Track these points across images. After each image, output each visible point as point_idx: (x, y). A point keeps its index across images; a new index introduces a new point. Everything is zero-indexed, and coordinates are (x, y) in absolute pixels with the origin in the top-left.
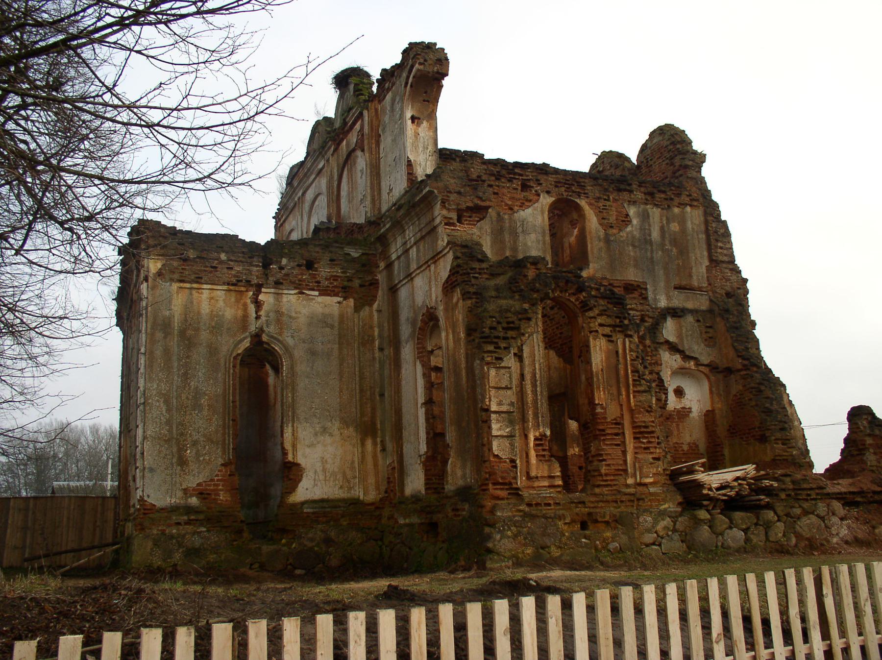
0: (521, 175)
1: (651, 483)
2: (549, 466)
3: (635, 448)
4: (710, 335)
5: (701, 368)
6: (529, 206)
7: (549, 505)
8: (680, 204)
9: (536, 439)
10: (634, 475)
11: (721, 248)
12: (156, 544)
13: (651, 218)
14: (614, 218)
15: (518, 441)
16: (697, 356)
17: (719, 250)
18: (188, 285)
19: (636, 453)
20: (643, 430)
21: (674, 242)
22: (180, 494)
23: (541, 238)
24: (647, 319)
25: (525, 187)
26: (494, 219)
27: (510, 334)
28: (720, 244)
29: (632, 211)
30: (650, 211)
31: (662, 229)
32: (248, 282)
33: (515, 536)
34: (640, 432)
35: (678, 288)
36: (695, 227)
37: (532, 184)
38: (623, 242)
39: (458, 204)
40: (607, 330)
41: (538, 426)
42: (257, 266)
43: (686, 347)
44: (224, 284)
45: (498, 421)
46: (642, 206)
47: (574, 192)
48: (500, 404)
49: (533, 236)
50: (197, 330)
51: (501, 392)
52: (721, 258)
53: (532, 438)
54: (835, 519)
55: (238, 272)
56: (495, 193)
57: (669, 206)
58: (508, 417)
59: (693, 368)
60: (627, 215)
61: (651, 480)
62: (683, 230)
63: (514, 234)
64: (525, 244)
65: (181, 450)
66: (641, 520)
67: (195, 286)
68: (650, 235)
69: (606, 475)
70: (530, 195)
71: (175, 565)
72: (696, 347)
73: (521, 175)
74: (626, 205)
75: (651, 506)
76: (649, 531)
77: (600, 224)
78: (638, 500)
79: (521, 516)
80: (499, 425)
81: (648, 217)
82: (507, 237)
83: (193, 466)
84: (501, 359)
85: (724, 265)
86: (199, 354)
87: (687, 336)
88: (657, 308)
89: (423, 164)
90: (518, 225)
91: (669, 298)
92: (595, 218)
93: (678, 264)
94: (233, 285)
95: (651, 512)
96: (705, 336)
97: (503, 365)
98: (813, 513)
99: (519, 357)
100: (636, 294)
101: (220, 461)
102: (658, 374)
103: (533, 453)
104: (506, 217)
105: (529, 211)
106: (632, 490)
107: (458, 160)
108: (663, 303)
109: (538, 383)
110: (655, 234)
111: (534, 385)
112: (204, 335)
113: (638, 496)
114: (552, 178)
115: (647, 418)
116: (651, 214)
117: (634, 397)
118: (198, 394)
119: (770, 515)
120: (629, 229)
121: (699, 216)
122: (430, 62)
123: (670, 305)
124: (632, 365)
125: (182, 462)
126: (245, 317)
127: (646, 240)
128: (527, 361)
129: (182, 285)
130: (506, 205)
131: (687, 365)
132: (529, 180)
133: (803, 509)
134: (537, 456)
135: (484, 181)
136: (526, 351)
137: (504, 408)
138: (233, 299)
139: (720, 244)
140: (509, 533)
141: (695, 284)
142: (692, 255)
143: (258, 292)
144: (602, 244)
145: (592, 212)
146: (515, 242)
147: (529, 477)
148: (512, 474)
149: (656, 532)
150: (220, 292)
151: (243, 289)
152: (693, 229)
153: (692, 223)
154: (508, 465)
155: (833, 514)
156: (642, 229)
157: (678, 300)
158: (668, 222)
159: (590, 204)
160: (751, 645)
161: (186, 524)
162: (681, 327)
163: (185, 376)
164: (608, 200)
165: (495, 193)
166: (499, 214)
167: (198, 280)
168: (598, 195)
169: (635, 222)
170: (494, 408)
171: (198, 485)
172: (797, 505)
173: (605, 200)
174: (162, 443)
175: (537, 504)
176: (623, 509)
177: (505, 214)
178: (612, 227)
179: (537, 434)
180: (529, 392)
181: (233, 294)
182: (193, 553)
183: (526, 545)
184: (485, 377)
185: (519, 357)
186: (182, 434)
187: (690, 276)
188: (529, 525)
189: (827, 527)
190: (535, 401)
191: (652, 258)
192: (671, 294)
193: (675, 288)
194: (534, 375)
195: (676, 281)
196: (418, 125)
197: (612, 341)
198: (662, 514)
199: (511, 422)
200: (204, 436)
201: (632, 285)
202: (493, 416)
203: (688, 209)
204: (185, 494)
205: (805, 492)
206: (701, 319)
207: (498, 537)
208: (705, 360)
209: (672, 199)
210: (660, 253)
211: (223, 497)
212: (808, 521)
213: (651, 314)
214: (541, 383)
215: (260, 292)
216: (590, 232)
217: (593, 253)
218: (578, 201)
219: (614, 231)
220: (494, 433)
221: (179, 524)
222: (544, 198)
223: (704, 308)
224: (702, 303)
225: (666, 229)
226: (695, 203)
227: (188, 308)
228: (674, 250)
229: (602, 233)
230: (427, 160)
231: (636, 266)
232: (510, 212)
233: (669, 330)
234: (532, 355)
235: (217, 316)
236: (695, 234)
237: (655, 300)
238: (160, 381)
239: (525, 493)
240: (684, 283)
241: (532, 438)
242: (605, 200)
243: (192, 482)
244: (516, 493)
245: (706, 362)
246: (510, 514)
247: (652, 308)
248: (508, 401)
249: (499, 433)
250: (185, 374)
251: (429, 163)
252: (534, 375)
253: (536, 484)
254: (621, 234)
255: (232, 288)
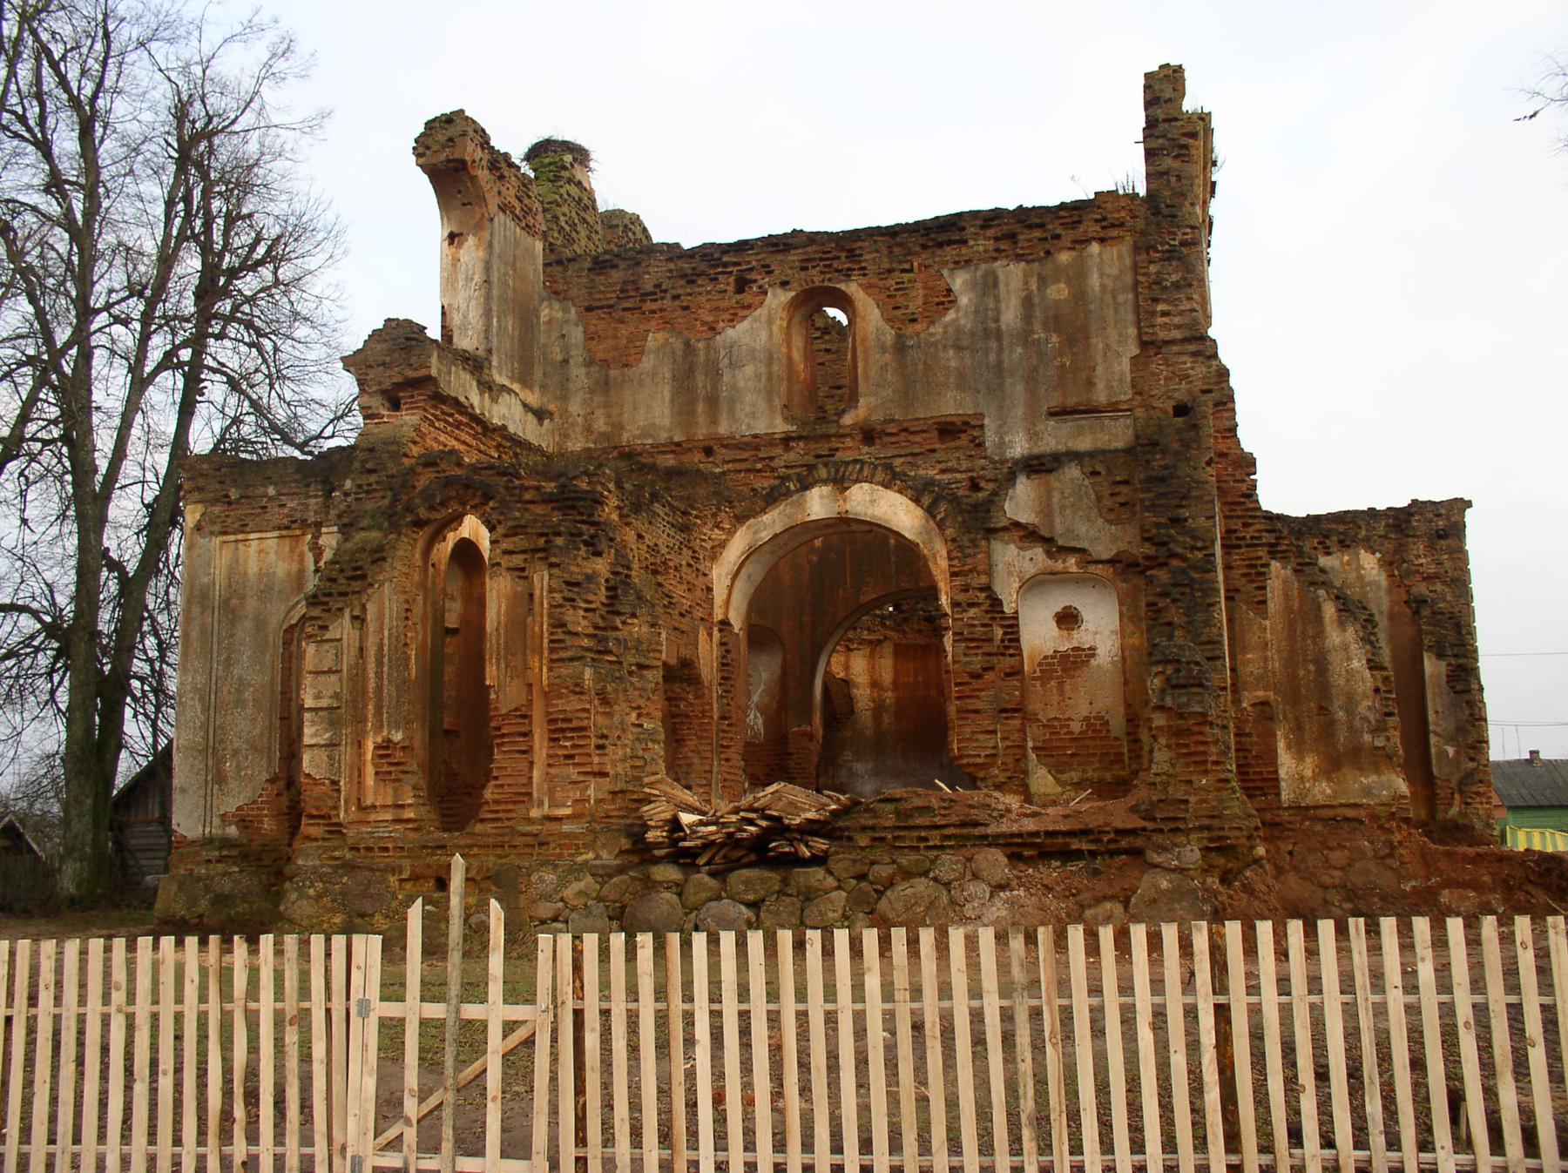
0: (738, 264)
1: (568, 817)
2: (395, 790)
3: (550, 756)
4: (1121, 499)
5: (1097, 569)
6: (745, 317)
7: (386, 849)
8: (1076, 242)
9: (377, 747)
10: (541, 804)
11: (1164, 314)
12: (181, 886)
13: (1002, 287)
14: (920, 302)
15: (346, 753)
16: (1085, 545)
17: (1160, 320)
18: (232, 538)
19: (549, 765)
20: (560, 725)
21: (1055, 322)
22: (216, 821)
23: (763, 369)
24: (983, 484)
25: (742, 285)
26: (680, 353)
27: (356, 585)
28: (1160, 307)
29: (959, 281)
30: (1000, 272)
31: (1027, 302)
32: (304, 521)
33: (319, 897)
34: (559, 729)
35: (1058, 413)
36: (1110, 285)
37: (753, 276)
38: (935, 344)
39: (380, 383)
40: (518, 560)
41: (382, 727)
42: (316, 496)
43: (1059, 528)
44: (274, 529)
45: (313, 723)
46: (983, 267)
47: (837, 271)
48: (318, 696)
49: (749, 370)
50: (242, 597)
51: (322, 678)
52: (1163, 335)
53: (370, 746)
54: (982, 889)
55: (292, 509)
56: (685, 308)
57: (1048, 253)
58: (331, 717)
59: (1074, 569)
60: (949, 291)
61: (568, 811)
62: (1080, 296)
63: (714, 372)
64: (734, 387)
65: (219, 762)
66: (534, 878)
67: (240, 537)
68: (997, 320)
69: (496, 802)
70: (746, 298)
71: (201, 916)
72: (1082, 528)
73: (738, 264)
74: (945, 272)
75: (560, 856)
76: (547, 897)
77: (888, 321)
78: (541, 844)
79: (331, 866)
80: (313, 730)
81: (996, 284)
82: (700, 379)
83: (233, 784)
84: (325, 628)
85: (1175, 348)
86: (244, 631)
87: (1063, 508)
88: (1003, 462)
89: (463, 307)
90: (722, 353)
91: (1033, 436)
92: (877, 312)
93: (1063, 365)
94: (288, 528)
95: (556, 866)
96: (1107, 502)
97: (327, 636)
98: (925, 874)
99: (359, 619)
100: (964, 440)
101: (265, 776)
102: (987, 588)
103: (370, 771)
104: (701, 345)
105: (744, 326)
106: (535, 829)
107: (622, 265)
108: (1019, 447)
109: (386, 660)
110: (1010, 316)
111: (380, 663)
112: (251, 604)
113: (541, 839)
114: (794, 257)
115: (571, 704)
116: (1001, 277)
117: (550, 669)
118: (242, 685)
119: (817, 875)
120: (950, 316)
121: (1120, 256)
122: (435, 148)
123: (1036, 451)
124: (550, 616)
125: (220, 779)
126: (301, 572)
127: (989, 331)
128: (371, 626)
129: (225, 538)
130: (704, 323)
131: (1059, 566)
132: (752, 269)
133: (900, 867)
134: (377, 773)
135: (665, 291)
136: (371, 609)
137: (324, 703)
138: (287, 549)
139: (1160, 307)
140: (311, 892)
141: (1101, 396)
142: (1098, 344)
143: (316, 537)
144: (888, 357)
145: (870, 300)
146: (714, 387)
147: (361, 808)
148: (330, 803)
149: (562, 900)
150: (271, 541)
151: (298, 532)
152: (1103, 286)
153: (1101, 275)
154: (326, 788)
155: (976, 876)
156: (979, 311)
157: (1055, 437)
158: (1043, 282)
159: (867, 288)
160: (1463, 1143)
161: (218, 861)
162: (1049, 492)
163: (228, 663)
164: (911, 270)
165: (685, 308)
166: (687, 344)
167: (243, 529)
168: (887, 266)
169: (964, 300)
170: (309, 702)
171: (238, 809)
172: (887, 859)
173: (903, 271)
174: (195, 754)
175: (369, 849)
176: (513, 859)
177: (698, 340)
178: (914, 320)
179: (379, 740)
180: (372, 675)
181: (287, 541)
182: (221, 900)
183: (334, 911)
184: (301, 655)
185: (359, 619)
186: (222, 741)
187: (1090, 383)
188: (345, 880)
189: (953, 902)
190: (379, 689)
191: (1000, 362)
192: (1040, 427)
193: (1052, 414)
194: (381, 646)
195: (1054, 400)
196: (460, 246)
197: (526, 578)
198: (577, 870)
199: (333, 724)
200: (247, 742)
201: (952, 423)
202: (307, 715)
203: (1095, 248)
204: (223, 821)
205: (915, 834)
206: (1100, 468)
207: (294, 896)
208: (1104, 550)
209: (1057, 237)
210: (1019, 350)
211: (268, 825)
212: (909, 891)
213: (989, 474)
214: (390, 660)
215: (320, 534)
216: (864, 340)
217: (867, 377)
218: (842, 286)
219: (918, 327)
220: (307, 740)
221: (209, 861)
222: (774, 295)
223: (1120, 445)
224: (1117, 434)
225: (1036, 300)
226: (1114, 233)
227: (232, 569)
228: (1055, 338)
229: (889, 335)
230: (470, 298)
231: (961, 386)
232: (710, 334)
233: (1021, 502)
234: (380, 617)
235: (268, 575)
236: (1108, 298)
237: (1002, 445)
238: (196, 671)
239: (351, 833)
240: (1072, 401)
241: (370, 746)
242: (903, 271)
243: (231, 804)
244: (336, 830)
245: (1106, 556)
246: (318, 862)
247: (993, 462)
248: (331, 692)
249: (313, 742)
250: (228, 659)
251: (473, 303)
252: (381, 646)
253: (373, 817)
254: (932, 330)
255: (284, 533)
